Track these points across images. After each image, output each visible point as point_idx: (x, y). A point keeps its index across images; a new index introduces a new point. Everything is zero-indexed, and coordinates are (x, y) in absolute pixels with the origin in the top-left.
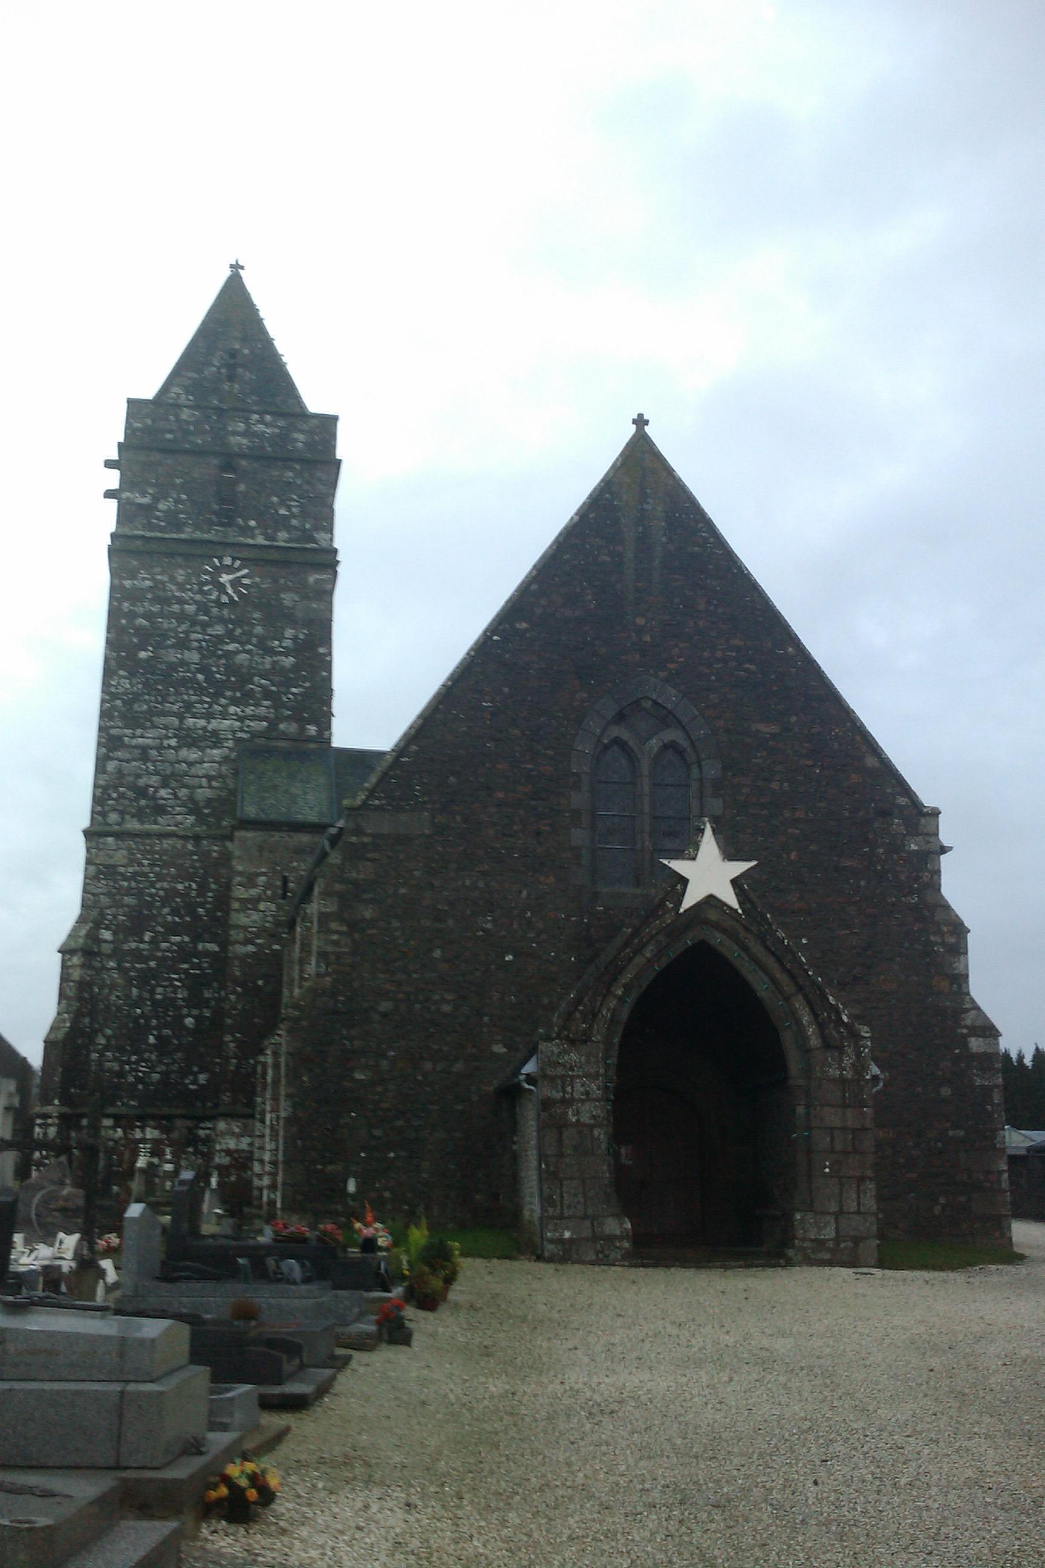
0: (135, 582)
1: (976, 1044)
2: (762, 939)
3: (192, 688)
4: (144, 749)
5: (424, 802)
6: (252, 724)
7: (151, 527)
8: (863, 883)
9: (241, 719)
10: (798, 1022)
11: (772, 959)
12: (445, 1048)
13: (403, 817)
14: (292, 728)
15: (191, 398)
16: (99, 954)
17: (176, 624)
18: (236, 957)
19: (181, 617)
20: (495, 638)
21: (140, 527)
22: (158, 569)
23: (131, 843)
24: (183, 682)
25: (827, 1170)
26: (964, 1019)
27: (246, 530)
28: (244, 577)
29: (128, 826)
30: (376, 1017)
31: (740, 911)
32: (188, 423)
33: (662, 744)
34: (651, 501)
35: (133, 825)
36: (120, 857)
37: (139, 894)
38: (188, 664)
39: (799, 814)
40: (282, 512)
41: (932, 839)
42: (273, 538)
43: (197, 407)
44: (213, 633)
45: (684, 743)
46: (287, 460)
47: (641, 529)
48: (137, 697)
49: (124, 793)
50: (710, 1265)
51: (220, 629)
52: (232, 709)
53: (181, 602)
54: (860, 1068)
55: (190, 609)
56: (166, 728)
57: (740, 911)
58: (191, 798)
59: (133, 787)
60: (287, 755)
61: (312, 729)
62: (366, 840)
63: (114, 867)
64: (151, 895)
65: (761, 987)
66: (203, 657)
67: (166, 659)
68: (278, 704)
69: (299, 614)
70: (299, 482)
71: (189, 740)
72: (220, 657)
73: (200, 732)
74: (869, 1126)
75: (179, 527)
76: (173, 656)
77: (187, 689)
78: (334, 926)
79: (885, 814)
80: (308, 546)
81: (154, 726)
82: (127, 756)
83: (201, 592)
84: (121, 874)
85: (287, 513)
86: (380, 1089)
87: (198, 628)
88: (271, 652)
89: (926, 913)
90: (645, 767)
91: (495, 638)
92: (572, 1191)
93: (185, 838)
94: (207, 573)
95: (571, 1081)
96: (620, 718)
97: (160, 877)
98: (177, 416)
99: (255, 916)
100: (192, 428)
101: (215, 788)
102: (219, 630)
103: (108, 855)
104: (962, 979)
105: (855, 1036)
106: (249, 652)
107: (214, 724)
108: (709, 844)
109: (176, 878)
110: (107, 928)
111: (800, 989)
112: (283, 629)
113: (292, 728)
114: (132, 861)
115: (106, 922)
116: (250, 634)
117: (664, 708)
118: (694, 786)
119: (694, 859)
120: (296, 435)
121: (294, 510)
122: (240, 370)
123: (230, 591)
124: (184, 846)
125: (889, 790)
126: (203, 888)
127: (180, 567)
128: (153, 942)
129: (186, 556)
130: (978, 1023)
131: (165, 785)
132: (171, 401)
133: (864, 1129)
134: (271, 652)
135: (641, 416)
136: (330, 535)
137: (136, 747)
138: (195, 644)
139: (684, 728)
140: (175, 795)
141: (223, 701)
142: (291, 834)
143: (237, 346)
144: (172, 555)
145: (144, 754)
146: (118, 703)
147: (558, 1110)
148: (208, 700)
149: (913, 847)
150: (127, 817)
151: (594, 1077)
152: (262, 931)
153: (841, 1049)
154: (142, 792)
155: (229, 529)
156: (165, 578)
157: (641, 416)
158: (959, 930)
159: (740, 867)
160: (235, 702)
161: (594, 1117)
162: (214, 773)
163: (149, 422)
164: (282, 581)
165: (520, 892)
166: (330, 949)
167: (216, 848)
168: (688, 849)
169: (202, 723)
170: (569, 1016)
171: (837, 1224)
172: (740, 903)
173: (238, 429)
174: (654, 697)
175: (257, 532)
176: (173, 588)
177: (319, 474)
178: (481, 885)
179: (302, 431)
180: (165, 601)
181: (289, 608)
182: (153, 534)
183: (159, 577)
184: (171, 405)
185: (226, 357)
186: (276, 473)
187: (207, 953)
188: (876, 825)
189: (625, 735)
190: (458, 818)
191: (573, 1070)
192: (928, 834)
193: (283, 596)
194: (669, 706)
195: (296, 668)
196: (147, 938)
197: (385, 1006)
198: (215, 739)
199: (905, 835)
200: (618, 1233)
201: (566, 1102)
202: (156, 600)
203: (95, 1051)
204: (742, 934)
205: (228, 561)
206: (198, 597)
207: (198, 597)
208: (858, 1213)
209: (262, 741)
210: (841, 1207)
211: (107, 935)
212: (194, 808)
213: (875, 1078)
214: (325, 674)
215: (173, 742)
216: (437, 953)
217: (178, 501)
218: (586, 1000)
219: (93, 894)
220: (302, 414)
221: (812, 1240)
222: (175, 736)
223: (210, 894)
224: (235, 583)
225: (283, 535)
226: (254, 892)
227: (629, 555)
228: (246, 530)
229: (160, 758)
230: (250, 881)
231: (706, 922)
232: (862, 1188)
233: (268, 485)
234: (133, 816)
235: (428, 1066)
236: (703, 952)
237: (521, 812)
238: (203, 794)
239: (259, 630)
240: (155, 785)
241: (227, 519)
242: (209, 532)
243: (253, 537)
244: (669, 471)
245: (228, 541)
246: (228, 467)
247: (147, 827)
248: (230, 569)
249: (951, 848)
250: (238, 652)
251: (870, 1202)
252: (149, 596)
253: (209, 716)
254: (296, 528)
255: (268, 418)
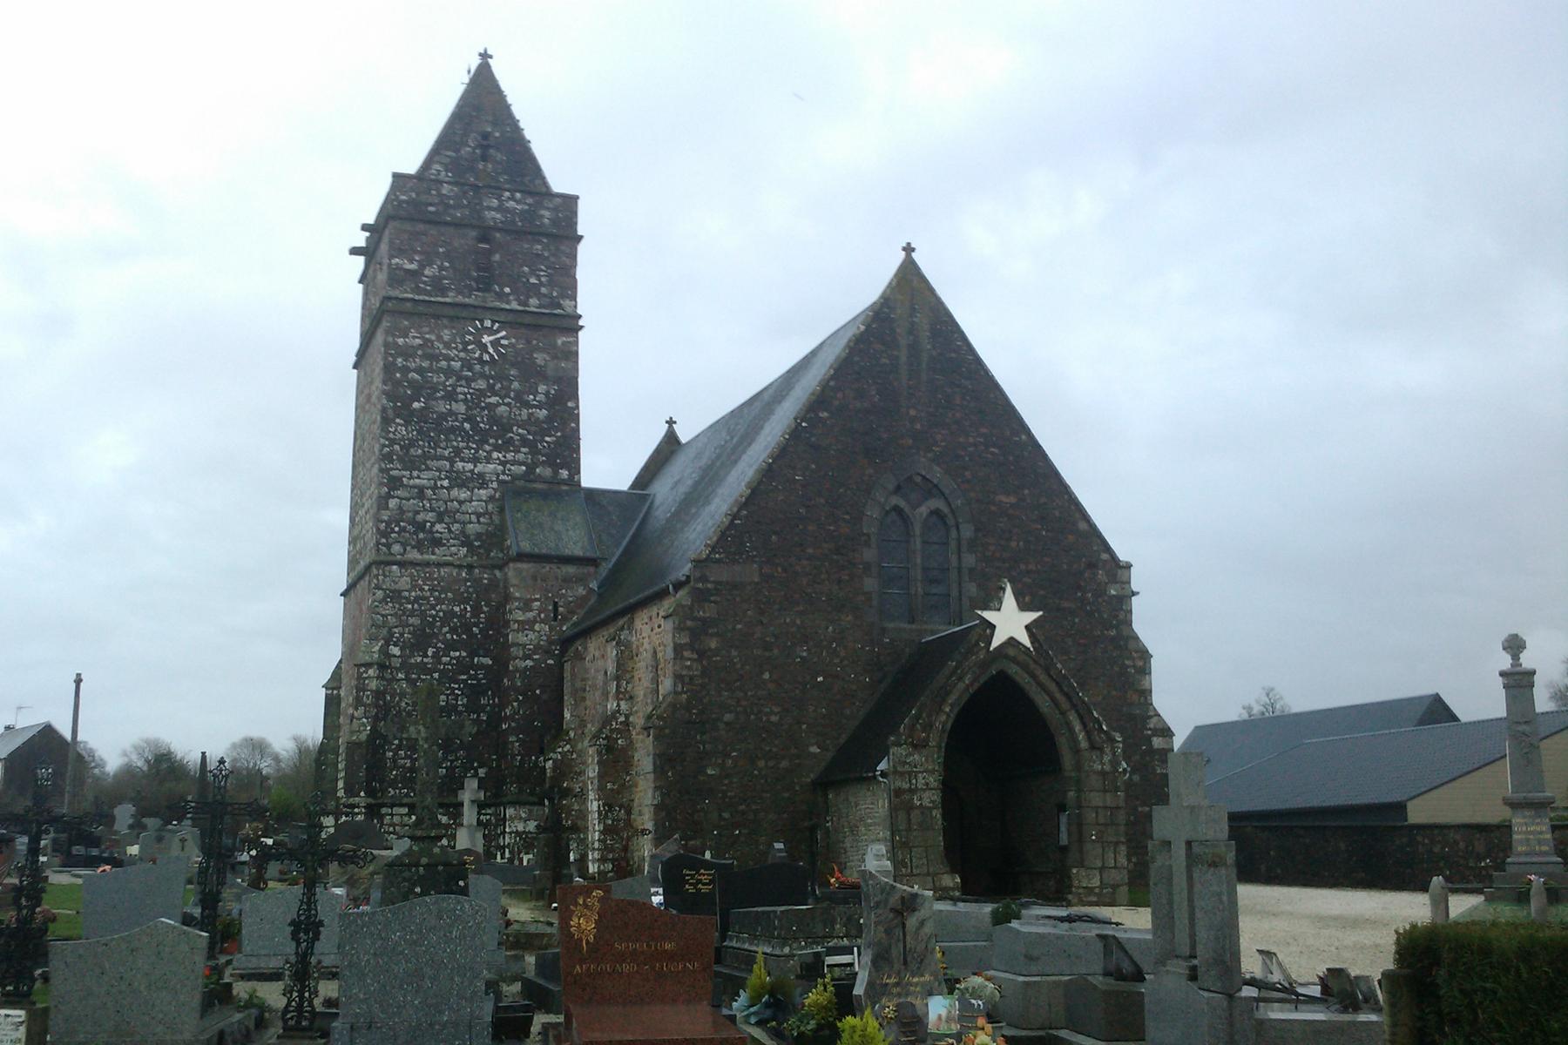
0: (407, 340)
1: (1157, 742)
2: (1047, 670)
3: (460, 435)
4: (421, 489)
5: (755, 556)
6: (512, 468)
7: (418, 290)
8: (1077, 620)
9: (503, 463)
10: (1071, 730)
11: (1054, 684)
12: (774, 750)
13: (737, 568)
14: (547, 472)
15: (450, 174)
16: (390, 667)
17: (444, 378)
18: (517, 670)
19: (449, 372)
20: (804, 424)
21: (408, 290)
22: (427, 329)
23: (413, 571)
24: (452, 430)
25: (1094, 837)
26: (1148, 724)
27: (501, 296)
28: (502, 338)
29: (409, 556)
30: (722, 726)
31: (1032, 649)
32: (449, 198)
33: (929, 511)
34: (918, 315)
35: (414, 555)
36: (404, 583)
37: (423, 615)
38: (456, 414)
39: (1032, 567)
40: (533, 280)
41: (1127, 586)
42: (526, 304)
43: (456, 184)
44: (477, 387)
45: (946, 510)
46: (536, 234)
47: (911, 338)
48: (412, 443)
49: (405, 527)
50: (1058, 904)
51: (482, 383)
52: (495, 455)
53: (448, 359)
54: (1115, 763)
55: (457, 365)
56: (439, 470)
57: (1032, 649)
58: (463, 532)
59: (413, 522)
60: (545, 496)
61: (564, 473)
62: (709, 586)
63: (400, 592)
64: (434, 617)
65: (1043, 703)
66: (469, 408)
67: (436, 409)
68: (534, 451)
69: (550, 372)
70: (546, 254)
71: (459, 481)
72: (483, 409)
73: (469, 474)
74: (1120, 805)
75: (443, 291)
76: (442, 407)
77: (456, 436)
78: (687, 654)
79: (1092, 566)
80: (555, 312)
81: (428, 469)
82: (406, 494)
83: (465, 350)
84: (406, 598)
85: (537, 282)
86: (726, 782)
87: (463, 383)
88: (527, 405)
89: (1122, 643)
90: (918, 531)
91: (804, 424)
92: (918, 856)
93: (460, 567)
94: (471, 334)
95: (916, 776)
96: (898, 489)
97: (439, 601)
98: (438, 190)
99: (532, 636)
100: (451, 202)
101: (484, 524)
102: (481, 384)
103: (393, 581)
104: (1146, 693)
105: (1112, 740)
106: (508, 405)
107: (480, 468)
108: (1009, 599)
109: (453, 601)
110: (395, 645)
111: (1074, 706)
112: (537, 385)
113: (547, 472)
114: (414, 587)
115: (394, 639)
116: (509, 389)
117: (931, 482)
118: (953, 544)
119: (999, 610)
120: (543, 212)
121: (543, 279)
122: (492, 151)
123: (491, 350)
124: (459, 574)
125: (1095, 548)
126: (476, 610)
127: (446, 327)
128: (435, 655)
129: (451, 318)
130: (1160, 726)
131: (441, 521)
132: (433, 177)
133: (1118, 808)
134: (527, 405)
135: (909, 244)
136: (574, 303)
137: (414, 487)
138: (462, 397)
139: (946, 499)
140: (450, 531)
141: (487, 448)
142: (560, 566)
143: (489, 130)
144: (437, 317)
145: (421, 493)
146: (397, 447)
147: (906, 797)
148: (474, 446)
149: (1113, 592)
150: (408, 548)
151: (932, 772)
152: (537, 648)
153: (1101, 749)
154: (420, 527)
155: (487, 295)
156: (433, 338)
157: (909, 244)
158: (1145, 655)
159: (1032, 616)
160: (497, 448)
161: (932, 802)
162: (482, 511)
163: (414, 195)
164: (535, 342)
165: (828, 628)
166: (684, 673)
167: (486, 576)
168: (994, 602)
169: (470, 466)
170: (912, 727)
171: (1101, 876)
172: (1032, 643)
173: (492, 204)
174: (924, 473)
175: (511, 298)
176: (441, 346)
177: (563, 248)
178: (798, 622)
179: (548, 209)
180: (434, 358)
181: (540, 366)
182: (421, 298)
183: (427, 336)
184: (432, 180)
185: (479, 138)
186: (526, 246)
187: (481, 666)
188: (1086, 575)
189: (902, 504)
190: (780, 570)
191: (916, 768)
192: (1123, 583)
193: (535, 356)
194: (935, 481)
195: (549, 419)
196: (430, 653)
197: (728, 717)
198: (481, 481)
199: (1106, 584)
200: (951, 885)
201: (912, 791)
202: (425, 357)
203: (390, 750)
204: (1032, 666)
205: (488, 323)
206: (462, 355)
207: (462, 355)
208: (1115, 867)
209: (521, 483)
210: (1103, 863)
211: (396, 651)
212: (466, 542)
213: (1125, 770)
214: (573, 425)
215: (446, 483)
216: (766, 676)
217: (441, 268)
218: (924, 715)
219: (383, 616)
220: (548, 194)
221: (1084, 888)
222: (447, 477)
223: (482, 615)
224: (496, 343)
225: (533, 301)
226: (530, 615)
227: (903, 359)
228: (501, 296)
229: (434, 497)
230: (527, 606)
231: (1007, 657)
232: (1118, 850)
233: (520, 256)
234: (413, 547)
235: (761, 763)
236: (1003, 677)
237: (827, 564)
238: (472, 528)
239: (515, 385)
240: (432, 520)
241: (485, 285)
242: (469, 297)
243: (508, 302)
244: (932, 290)
245: (487, 306)
246: (484, 239)
247: (426, 557)
248: (491, 331)
249: (1138, 593)
250: (498, 405)
251: (1123, 861)
252: (420, 352)
253: (475, 460)
254: (545, 295)
255: (518, 195)
